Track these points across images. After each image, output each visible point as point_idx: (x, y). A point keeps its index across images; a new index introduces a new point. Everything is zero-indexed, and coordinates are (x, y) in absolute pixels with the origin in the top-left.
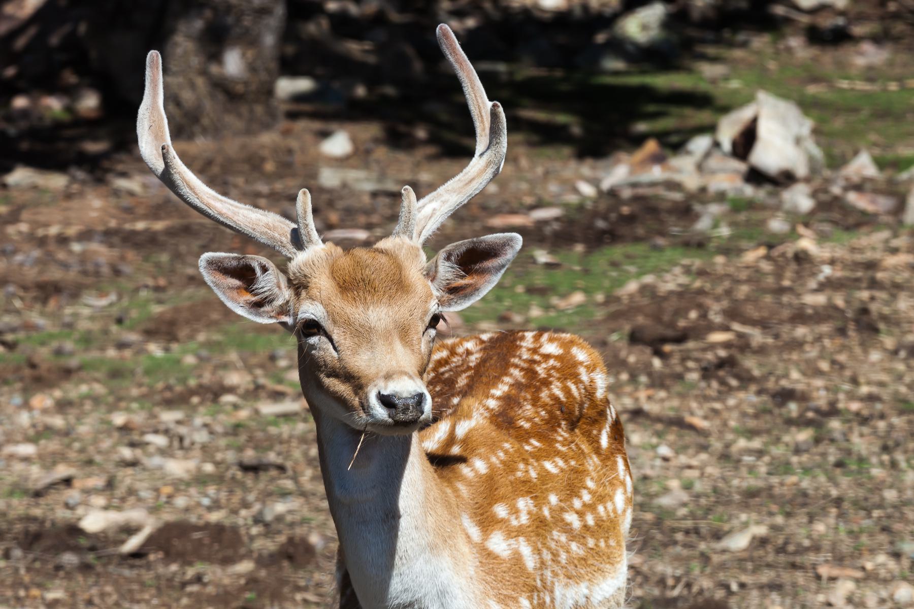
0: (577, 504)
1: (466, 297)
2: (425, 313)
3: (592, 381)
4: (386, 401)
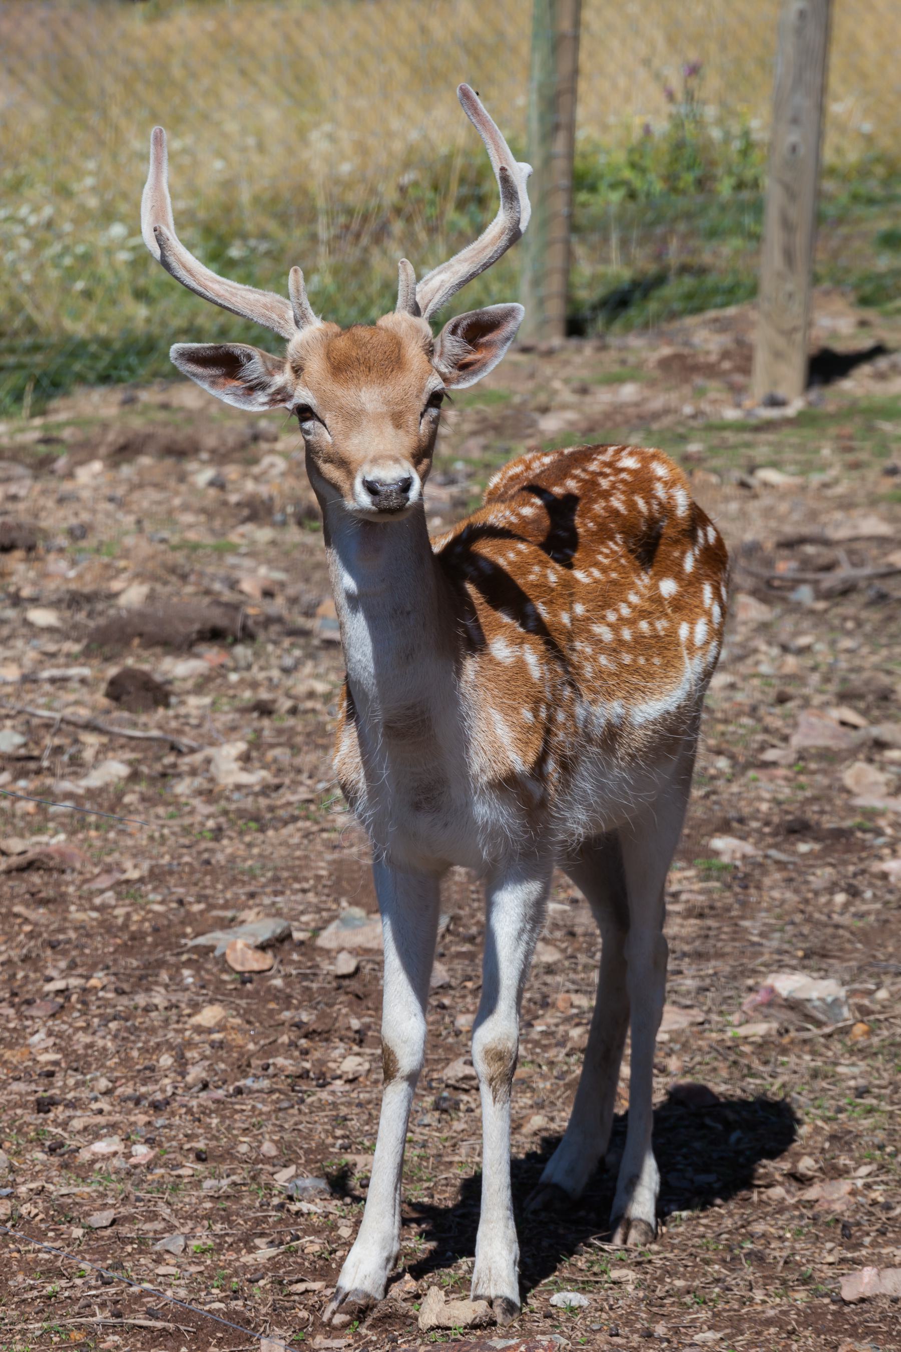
0: (612, 617)
1: (475, 373)
2: (421, 390)
3: (671, 497)
4: (371, 488)
